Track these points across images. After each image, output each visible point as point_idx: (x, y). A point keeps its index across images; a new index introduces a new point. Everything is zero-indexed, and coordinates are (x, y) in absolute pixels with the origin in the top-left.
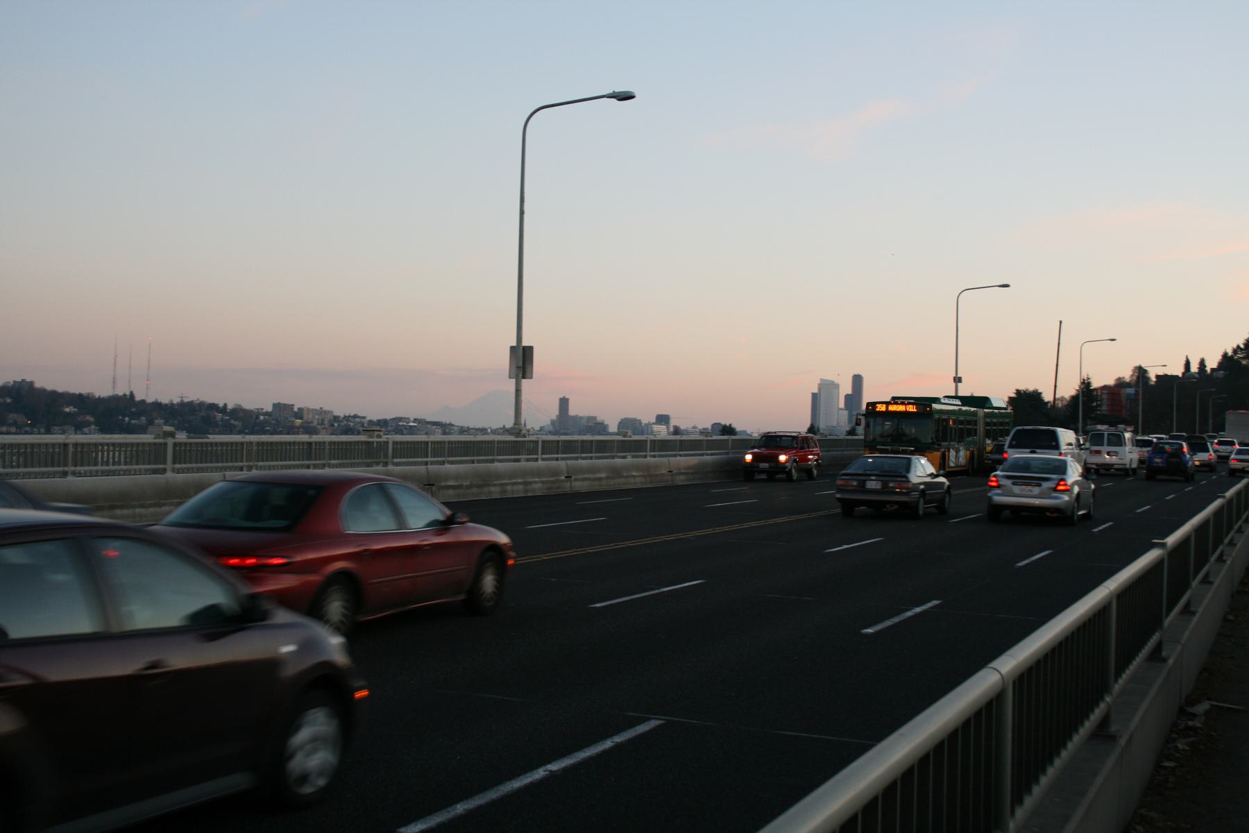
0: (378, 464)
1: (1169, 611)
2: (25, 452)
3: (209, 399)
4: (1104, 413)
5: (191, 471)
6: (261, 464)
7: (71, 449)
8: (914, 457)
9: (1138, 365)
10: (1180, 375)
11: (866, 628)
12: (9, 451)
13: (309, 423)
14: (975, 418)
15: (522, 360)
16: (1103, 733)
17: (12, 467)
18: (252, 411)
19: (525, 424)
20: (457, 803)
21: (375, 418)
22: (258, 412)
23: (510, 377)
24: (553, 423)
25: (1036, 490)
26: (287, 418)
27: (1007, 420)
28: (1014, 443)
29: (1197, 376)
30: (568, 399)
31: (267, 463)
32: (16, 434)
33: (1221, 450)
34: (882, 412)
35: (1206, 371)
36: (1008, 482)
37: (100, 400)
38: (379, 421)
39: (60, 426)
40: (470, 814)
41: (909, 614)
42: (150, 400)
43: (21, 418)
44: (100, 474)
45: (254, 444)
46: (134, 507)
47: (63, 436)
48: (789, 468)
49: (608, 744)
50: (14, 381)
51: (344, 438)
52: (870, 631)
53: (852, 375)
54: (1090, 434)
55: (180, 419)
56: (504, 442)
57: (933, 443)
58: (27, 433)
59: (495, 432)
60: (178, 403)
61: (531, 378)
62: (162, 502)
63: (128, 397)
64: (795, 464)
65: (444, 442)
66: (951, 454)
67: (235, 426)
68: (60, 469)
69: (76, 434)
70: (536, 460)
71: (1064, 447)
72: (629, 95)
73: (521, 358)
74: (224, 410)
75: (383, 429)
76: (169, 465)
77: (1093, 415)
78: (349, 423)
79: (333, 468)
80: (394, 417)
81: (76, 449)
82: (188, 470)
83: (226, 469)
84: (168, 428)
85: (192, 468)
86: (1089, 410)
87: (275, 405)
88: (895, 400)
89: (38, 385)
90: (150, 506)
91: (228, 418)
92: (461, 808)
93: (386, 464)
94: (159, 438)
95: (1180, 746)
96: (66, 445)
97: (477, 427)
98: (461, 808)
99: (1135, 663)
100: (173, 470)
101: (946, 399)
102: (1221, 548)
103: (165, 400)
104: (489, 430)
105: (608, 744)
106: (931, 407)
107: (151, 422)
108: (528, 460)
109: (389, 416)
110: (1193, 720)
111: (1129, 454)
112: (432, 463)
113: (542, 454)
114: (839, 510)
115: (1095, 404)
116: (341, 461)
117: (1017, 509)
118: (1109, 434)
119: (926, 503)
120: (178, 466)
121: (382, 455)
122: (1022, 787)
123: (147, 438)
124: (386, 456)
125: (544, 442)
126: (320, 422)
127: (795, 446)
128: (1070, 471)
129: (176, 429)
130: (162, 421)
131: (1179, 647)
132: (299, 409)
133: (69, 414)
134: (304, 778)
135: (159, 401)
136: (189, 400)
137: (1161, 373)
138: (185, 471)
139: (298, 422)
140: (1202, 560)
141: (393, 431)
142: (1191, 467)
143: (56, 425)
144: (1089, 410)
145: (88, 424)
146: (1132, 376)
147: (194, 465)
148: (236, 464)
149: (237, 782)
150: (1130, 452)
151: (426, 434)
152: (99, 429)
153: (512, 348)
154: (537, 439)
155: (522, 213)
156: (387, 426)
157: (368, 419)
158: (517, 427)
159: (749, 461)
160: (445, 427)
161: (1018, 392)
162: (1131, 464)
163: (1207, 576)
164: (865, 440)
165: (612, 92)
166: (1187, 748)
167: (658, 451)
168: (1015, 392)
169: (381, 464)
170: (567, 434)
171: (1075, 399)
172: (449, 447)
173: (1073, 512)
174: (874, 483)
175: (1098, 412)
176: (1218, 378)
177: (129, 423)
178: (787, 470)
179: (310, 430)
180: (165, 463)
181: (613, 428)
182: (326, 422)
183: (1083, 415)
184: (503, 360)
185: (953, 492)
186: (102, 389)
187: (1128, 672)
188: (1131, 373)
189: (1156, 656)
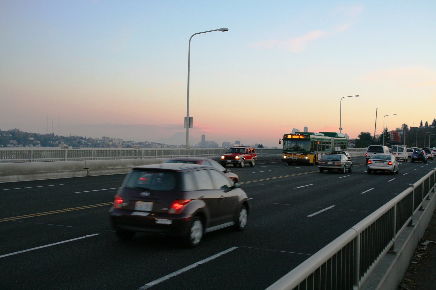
0: (139, 157)
1: (415, 210)
2: (16, 154)
3: (80, 135)
4: (392, 140)
5: (74, 160)
6: (98, 157)
7: (32, 152)
8: (342, 155)
9: (404, 123)
10: (419, 127)
12: (11, 153)
13: (114, 143)
14: (330, 141)
15: (189, 121)
16: (392, 252)
17: (12, 158)
18: (95, 139)
19: (190, 144)
20: (166, 275)
21: (137, 142)
22: (97, 140)
24: (200, 144)
25: (382, 164)
26: (107, 142)
27: (345, 142)
28: (369, 151)
29: (425, 127)
30: (205, 135)
31: (100, 157)
32: (13, 147)
33: (435, 153)
34: (290, 138)
35: (428, 126)
36: (374, 162)
42: (59, 135)
43: (15, 142)
44: (57, 161)
45: (96, 151)
46: (54, 172)
47: (29, 148)
48: (240, 162)
50: (13, 129)
51: (127, 149)
53: (304, 127)
54: (392, 148)
55: (70, 142)
56: (182, 150)
57: (310, 151)
58: (17, 147)
59: (179, 147)
60: (69, 137)
61: (192, 128)
62: (64, 171)
63: (52, 134)
64: (243, 160)
65: (162, 150)
66: (319, 156)
67: (89, 145)
68: (29, 159)
69: (34, 147)
72: (226, 29)
73: (189, 121)
74: (85, 139)
75: (140, 146)
76: (66, 158)
77: (388, 141)
78: (129, 144)
79: (123, 159)
80: (144, 141)
81: (34, 152)
82: (73, 160)
83: (86, 159)
84: (67, 145)
85: (74, 159)
86: (387, 139)
87: (103, 137)
89: (20, 130)
90: (59, 172)
91: (86, 142)
92: (167, 277)
93: (142, 158)
94: (63, 149)
95: (419, 256)
97: (173, 145)
98: (167, 277)
99: (381, 256)
100: (68, 160)
102: (433, 187)
103: (65, 136)
104: (177, 146)
105: (218, 255)
106: (309, 136)
107: (60, 143)
108: (191, 156)
110: (423, 247)
111: (405, 154)
112: (158, 157)
113: (196, 154)
114: (319, 171)
115: (389, 137)
116: (126, 157)
117: (375, 170)
118: (399, 148)
119: (346, 169)
120: (69, 158)
121: (140, 155)
122: (363, 271)
123: (58, 149)
124: (141, 155)
125: (196, 150)
126: (119, 143)
127: (244, 152)
128: (392, 159)
129: (69, 146)
130: (64, 143)
131: (418, 222)
132: (111, 139)
133: (31, 140)
134: (194, 239)
135: (63, 136)
136: (73, 135)
137: (412, 127)
138: (72, 160)
139: (111, 143)
140: (426, 192)
142: (426, 158)
143: (27, 144)
144: (387, 139)
145: (38, 144)
146: (402, 127)
148: (89, 158)
149: (230, 224)
150: (405, 154)
151: (155, 147)
152: (42, 146)
153: (185, 117)
154: (194, 149)
155: (189, 70)
156: (142, 145)
157: (135, 142)
158: (187, 145)
160: (162, 145)
161: (362, 133)
162: (406, 157)
163: (428, 197)
164: (283, 150)
165: (220, 28)
166: (421, 257)
167: (203, 154)
168: (361, 133)
169: (140, 158)
170: (204, 147)
171: (382, 135)
172: (163, 152)
173: (393, 171)
174: (330, 162)
175: (390, 140)
176: (432, 128)
177: (52, 143)
180: (65, 157)
181: (220, 145)
182: (121, 143)
183: (385, 141)
185: (353, 166)
186: (42, 131)
187: (400, 230)
188: (401, 126)
189: (410, 225)
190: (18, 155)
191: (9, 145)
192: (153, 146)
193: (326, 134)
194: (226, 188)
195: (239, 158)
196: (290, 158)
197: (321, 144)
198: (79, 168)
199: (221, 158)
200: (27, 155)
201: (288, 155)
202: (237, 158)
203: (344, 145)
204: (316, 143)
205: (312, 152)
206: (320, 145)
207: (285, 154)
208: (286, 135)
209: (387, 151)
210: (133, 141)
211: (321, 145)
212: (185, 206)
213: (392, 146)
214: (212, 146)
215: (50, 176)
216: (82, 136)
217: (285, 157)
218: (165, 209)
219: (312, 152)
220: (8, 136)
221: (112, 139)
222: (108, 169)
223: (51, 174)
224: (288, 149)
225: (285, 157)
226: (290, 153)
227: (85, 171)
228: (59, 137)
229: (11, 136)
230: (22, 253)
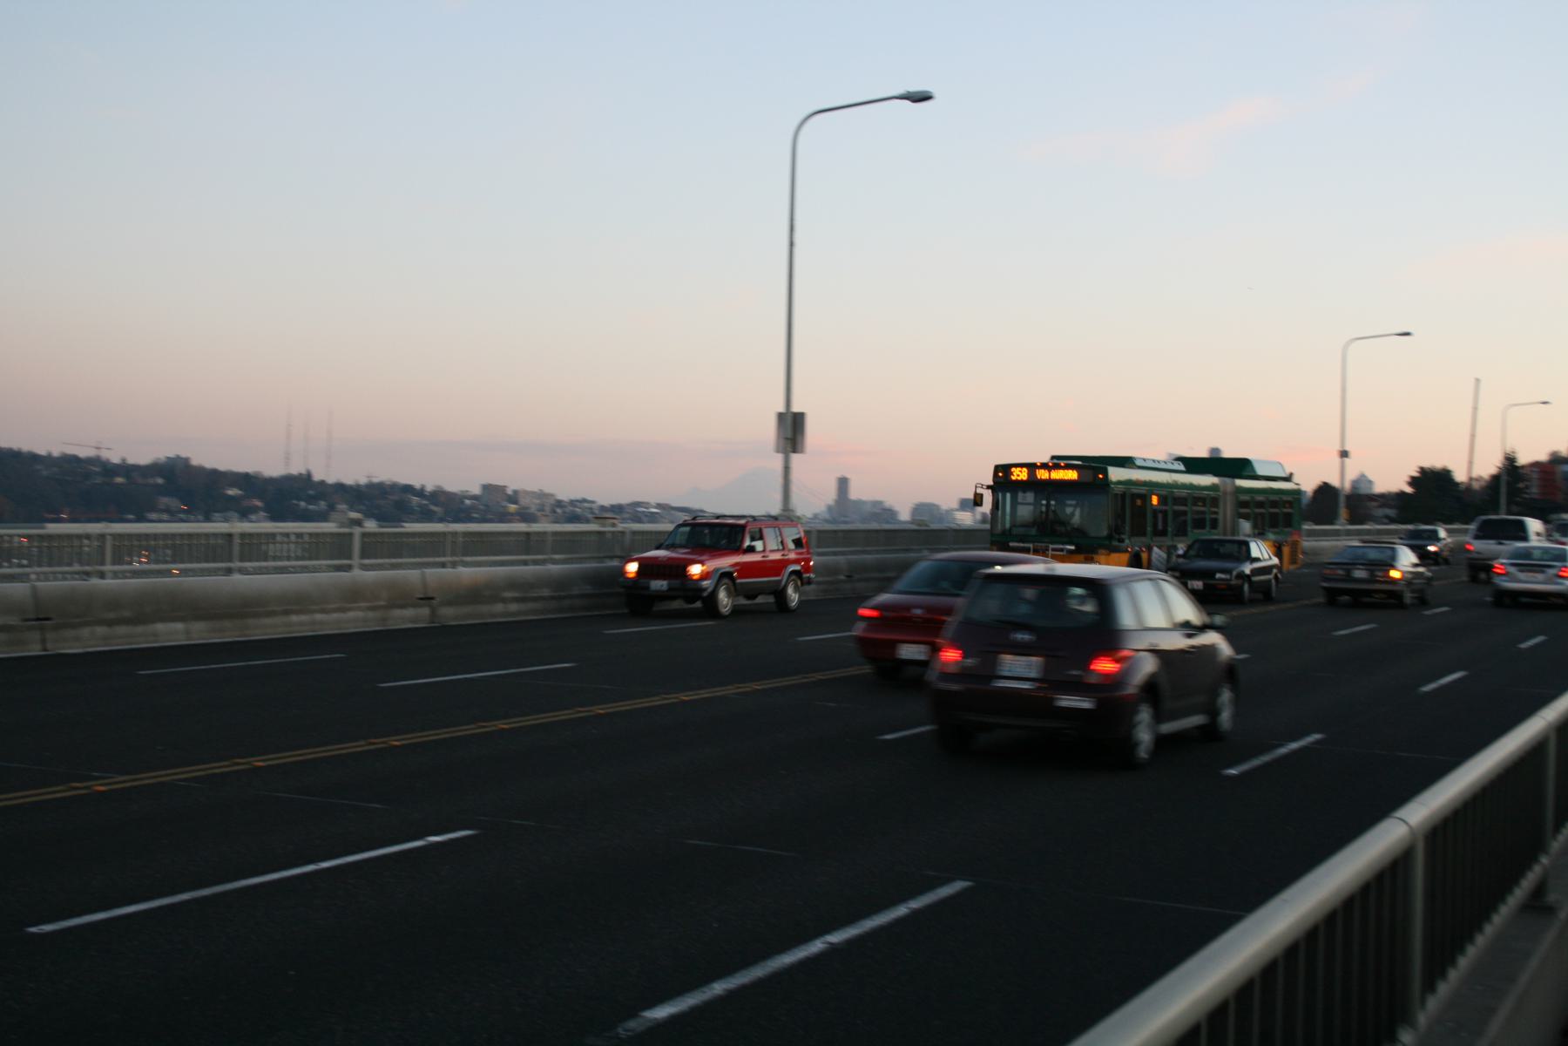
3: (403, 479)
7: (237, 541)
11: (1230, 766)
15: (792, 429)
16: (1538, 905)
21: (606, 502)
23: (778, 452)
24: (830, 508)
25: (1540, 577)
27: (1289, 498)
36: (1512, 570)
37: (271, 481)
38: (613, 506)
40: (731, 995)
41: (1283, 751)
42: (331, 480)
47: (226, 525)
48: (710, 590)
49: (901, 911)
52: (1233, 772)
57: (1110, 537)
67: (434, 512)
70: (349, 568)
71: (1533, 537)
74: (420, 493)
76: (356, 561)
77: (1518, 499)
84: (354, 515)
86: (1513, 492)
88: (1058, 462)
89: (195, 462)
92: (718, 988)
96: (230, 536)
98: (718, 988)
99: (1497, 919)
101: (1175, 463)
103: (349, 480)
105: (901, 911)
106: (1105, 473)
107: (332, 508)
109: (624, 499)
114: (1321, 600)
122: (1436, 969)
133: (232, 498)
139: (512, 507)
144: (1513, 492)
145: (255, 510)
147: (387, 561)
148: (437, 559)
158: (786, 513)
164: (991, 532)
168: (1419, 470)
170: (846, 522)
171: (1496, 479)
178: (705, 594)
179: (525, 517)
180: (350, 557)
186: (272, 468)
190: (182, 549)
191: (154, 516)
192: (662, 517)
193: (1193, 465)
194: (1188, 628)
195: (702, 571)
197: (1164, 508)
198: (401, 597)
199: (622, 572)
200: (218, 550)
202: (696, 570)
204: (1139, 502)
208: (1003, 471)
209: (1538, 534)
210: (590, 499)
211: (1165, 513)
212: (1125, 665)
213: (1554, 516)
214: (875, 516)
215: (300, 624)
216: (936, 502)
218: (1074, 673)
220: (151, 481)
221: (516, 492)
222: (504, 601)
223: (304, 618)
226: (1022, 545)
227: (421, 606)
228: (331, 485)
229: (160, 481)
230: (205, 898)
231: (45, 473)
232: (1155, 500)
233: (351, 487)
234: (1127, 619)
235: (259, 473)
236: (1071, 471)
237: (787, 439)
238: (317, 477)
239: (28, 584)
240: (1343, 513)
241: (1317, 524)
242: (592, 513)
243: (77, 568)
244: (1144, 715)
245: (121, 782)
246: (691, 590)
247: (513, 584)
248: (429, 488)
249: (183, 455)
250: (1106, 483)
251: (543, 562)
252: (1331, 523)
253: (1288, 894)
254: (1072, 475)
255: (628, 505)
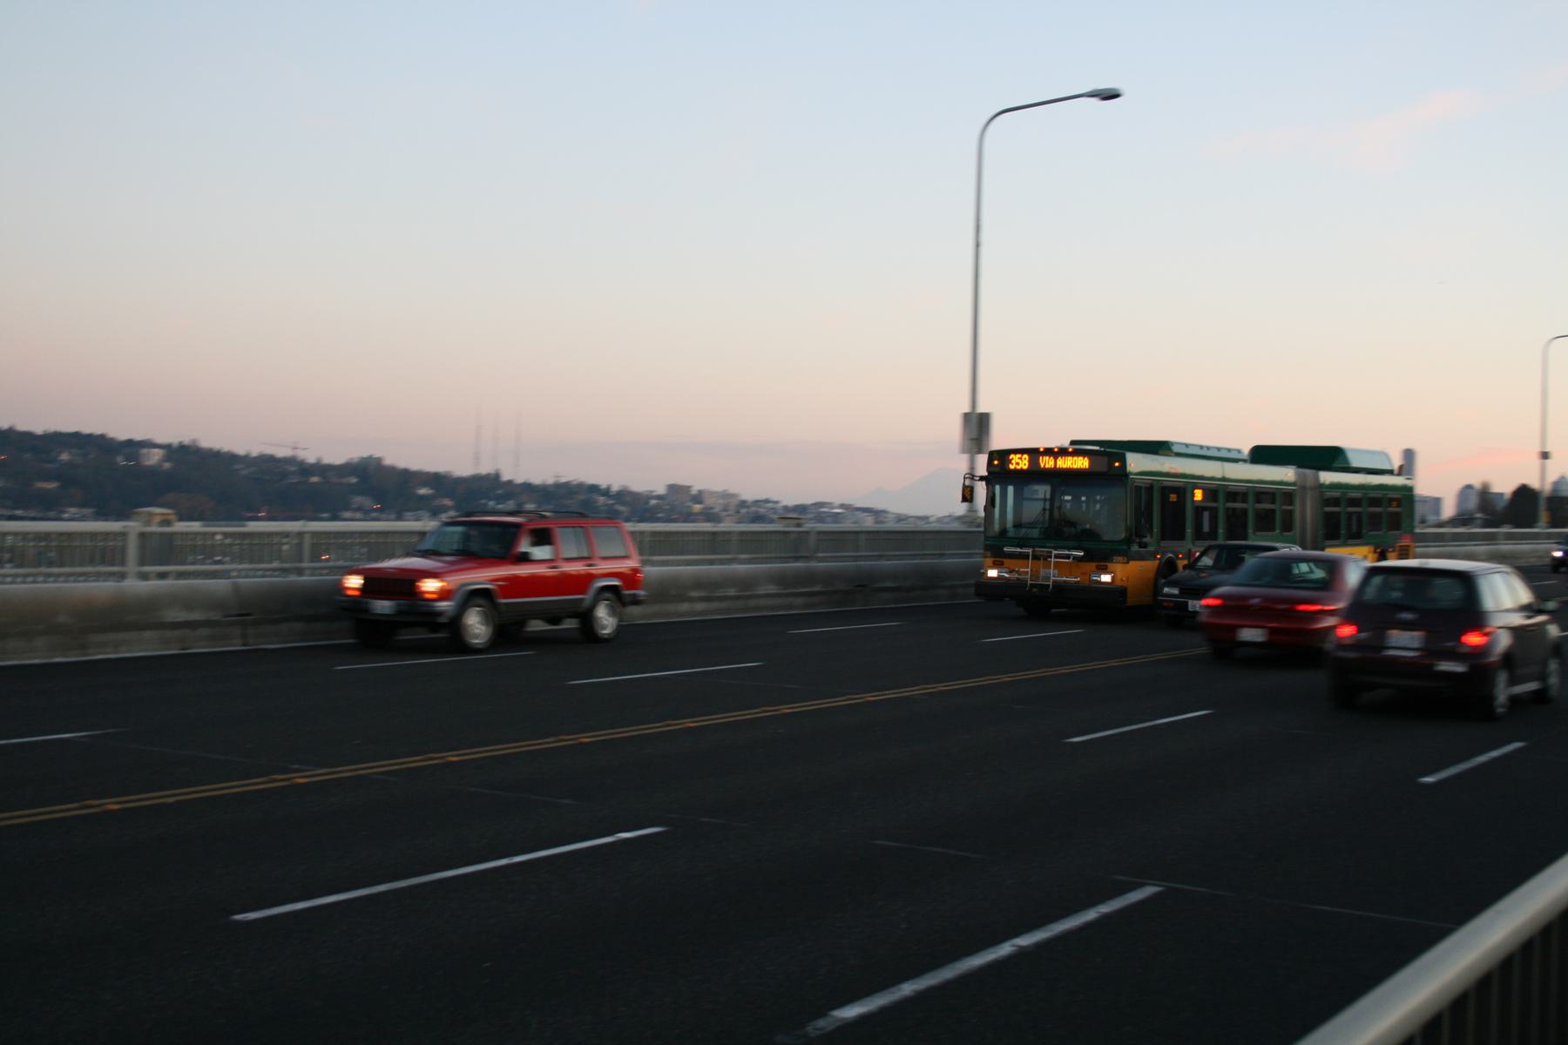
3: (590, 479)
11: (1425, 775)
13: (712, 508)
37: (461, 481)
39: (414, 511)
40: (921, 996)
42: (519, 480)
43: (366, 501)
47: (708, 524)
49: (1091, 915)
57: (1128, 541)
74: (606, 493)
76: (132, 566)
88: (1078, 448)
92: (907, 989)
98: (907, 989)
105: (1091, 915)
133: (423, 497)
139: (697, 507)
141: (612, 517)
143: (408, 511)
149: (1532, 686)
158: (970, 514)
159: (418, 587)
180: (123, 563)
184: (954, 431)
186: (462, 467)
191: (347, 514)
193: (1263, 455)
196: (1018, 579)
199: (340, 588)
201: (1007, 562)
202: (430, 586)
203: (1391, 509)
204: (1173, 497)
205: (1135, 548)
206: (1205, 509)
207: (991, 557)
217: (993, 573)
218: (1449, 644)
219: (1135, 548)
220: (345, 480)
221: (700, 492)
222: (692, 600)
224: (1011, 533)
225: (993, 573)
231: (244, 472)
232: (1198, 495)
233: (537, 486)
234: (1488, 603)
235: (449, 472)
236: (1081, 458)
237: (972, 439)
238: (505, 477)
239: (228, 581)
240: (1544, 516)
241: (1517, 526)
242: (775, 513)
243: (275, 565)
244: (1502, 678)
245: (321, 774)
246: (419, 612)
247: (699, 583)
248: (615, 488)
249: (377, 455)
250: (1122, 475)
251: (731, 561)
252: (1530, 526)
253: (1501, 906)
254: (1082, 463)
255: (813, 505)
